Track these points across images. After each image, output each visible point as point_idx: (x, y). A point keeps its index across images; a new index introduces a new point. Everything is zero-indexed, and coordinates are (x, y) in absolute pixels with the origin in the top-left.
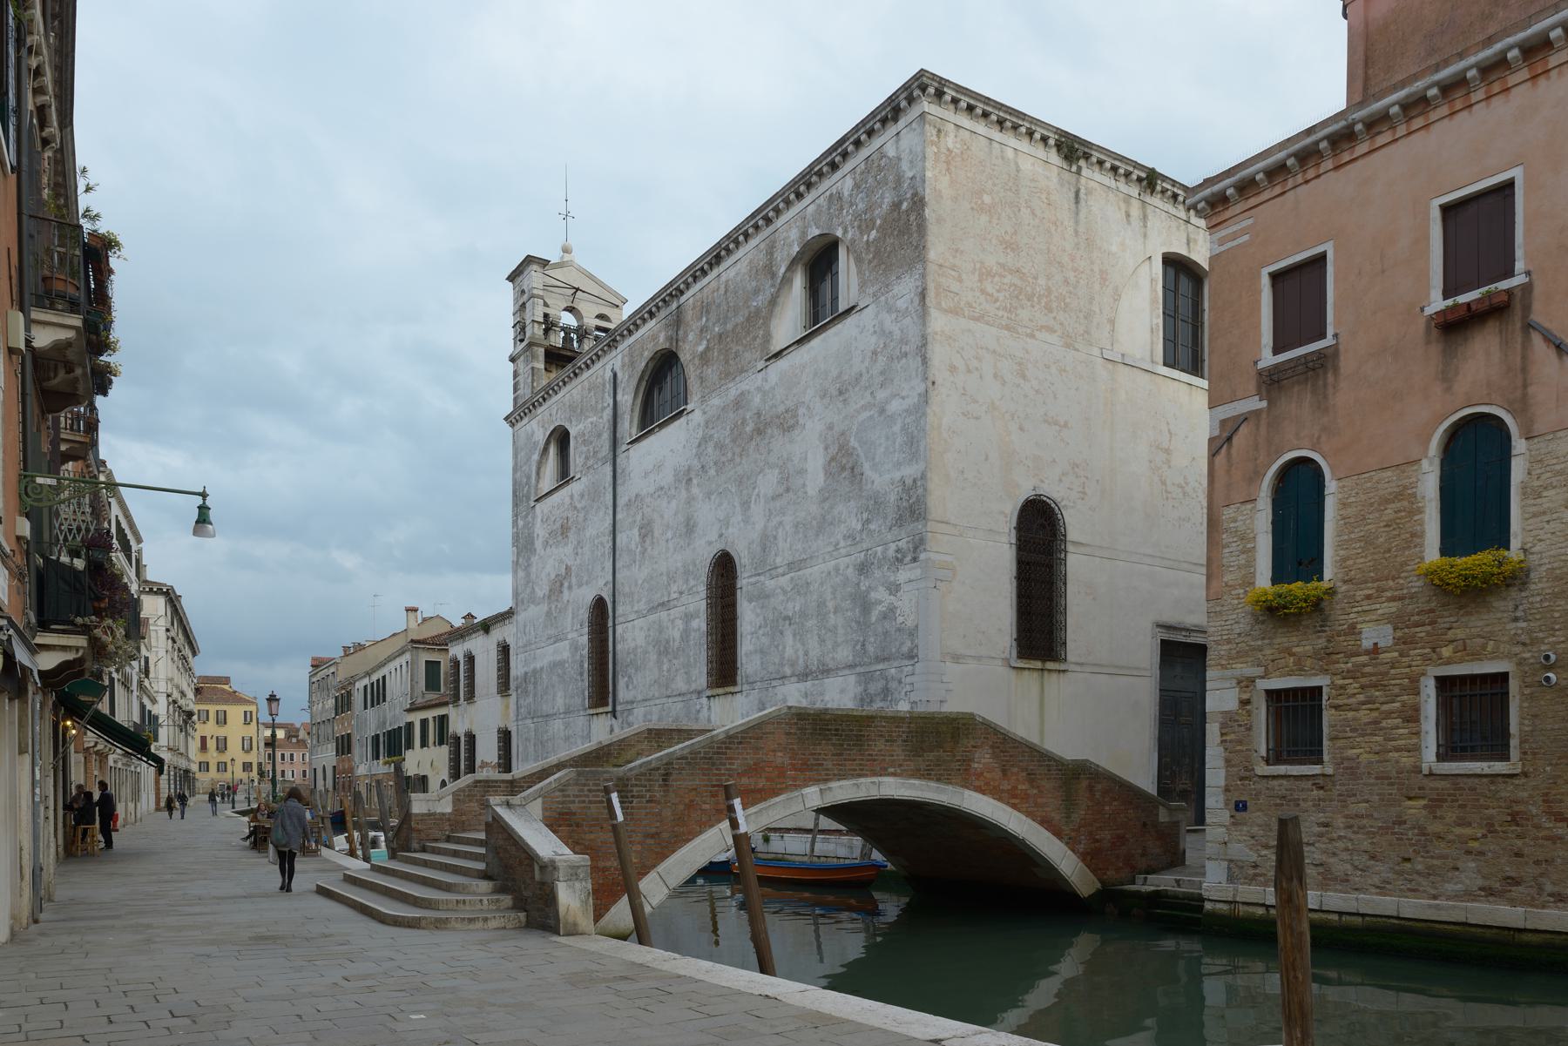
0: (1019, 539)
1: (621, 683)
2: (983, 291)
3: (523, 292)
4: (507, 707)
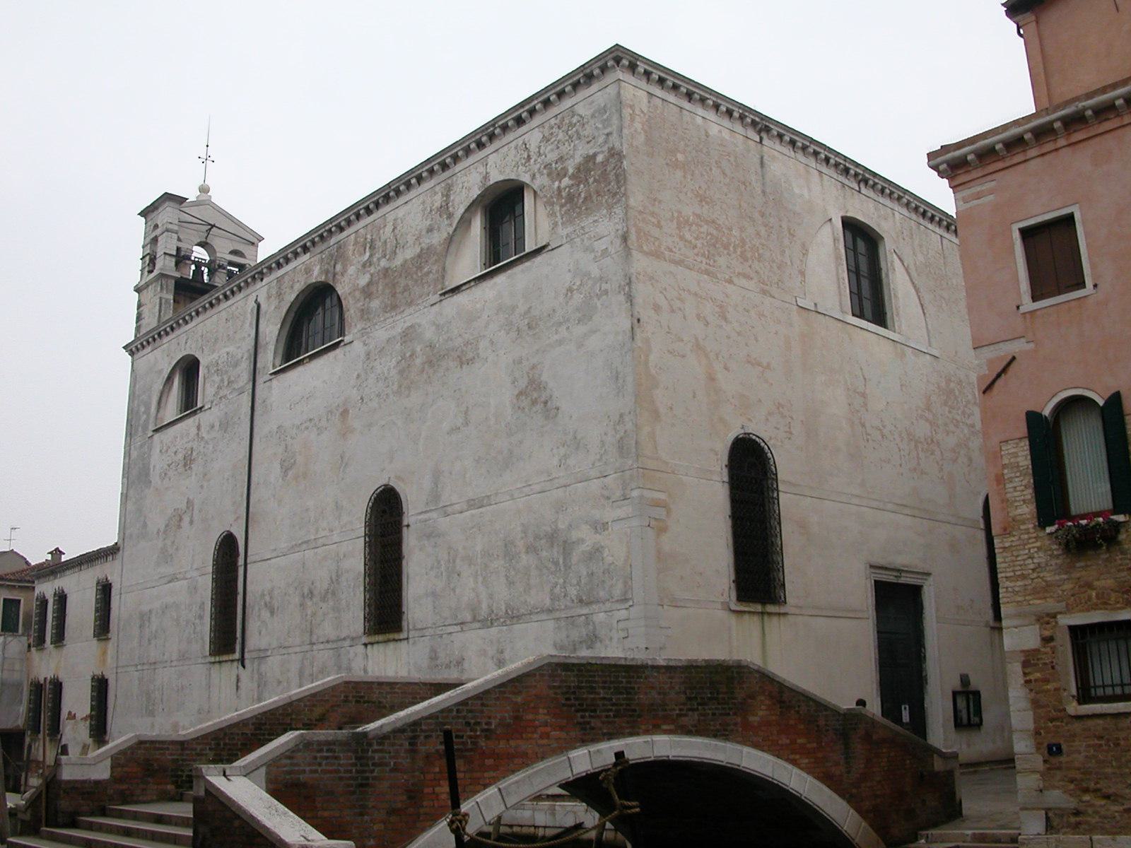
0: (731, 477)
1: (252, 626)
2: (682, 238)
3: (156, 226)
4: (104, 653)
